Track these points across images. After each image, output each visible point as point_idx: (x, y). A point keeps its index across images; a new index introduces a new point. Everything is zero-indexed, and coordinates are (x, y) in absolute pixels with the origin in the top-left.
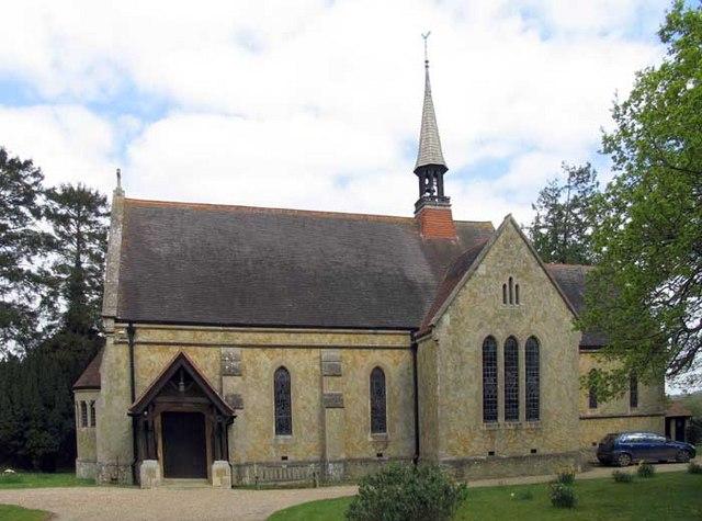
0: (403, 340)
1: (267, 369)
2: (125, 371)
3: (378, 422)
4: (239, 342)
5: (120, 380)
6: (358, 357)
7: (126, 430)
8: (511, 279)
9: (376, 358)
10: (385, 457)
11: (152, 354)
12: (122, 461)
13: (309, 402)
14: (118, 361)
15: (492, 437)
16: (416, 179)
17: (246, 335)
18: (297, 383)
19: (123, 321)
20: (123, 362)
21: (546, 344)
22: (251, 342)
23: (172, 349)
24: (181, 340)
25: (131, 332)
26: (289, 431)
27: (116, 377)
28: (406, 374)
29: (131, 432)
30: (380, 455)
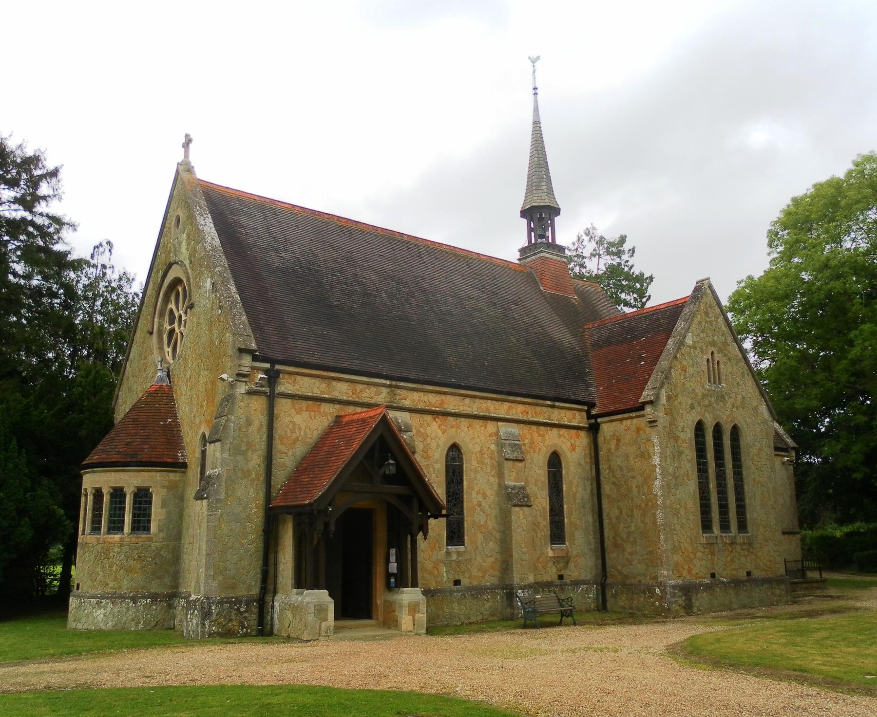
0: (578, 418)
1: (438, 446)
2: (259, 439)
3: (557, 534)
4: (407, 403)
5: (250, 454)
6: (535, 435)
7: (252, 537)
8: (712, 353)
9: (554, 439)
10: (567, 580)
11: (298, 413)
12: (242, 592)
13: (484, 495)
14: (249, 423)
15: (713, 554)
16: (524, 221)
17: (416, 396)
18: (470, 466)
19: (264, 360)
20: (256, 424)
21: (747, 437)
22: (420, 406)
23: (326, 407)
24: (336, 395)
25: (273, 377)
26: (461, 542)
27: (244, 448)
28: (583, 463)
29: (260, 544)
30: (561, 577)
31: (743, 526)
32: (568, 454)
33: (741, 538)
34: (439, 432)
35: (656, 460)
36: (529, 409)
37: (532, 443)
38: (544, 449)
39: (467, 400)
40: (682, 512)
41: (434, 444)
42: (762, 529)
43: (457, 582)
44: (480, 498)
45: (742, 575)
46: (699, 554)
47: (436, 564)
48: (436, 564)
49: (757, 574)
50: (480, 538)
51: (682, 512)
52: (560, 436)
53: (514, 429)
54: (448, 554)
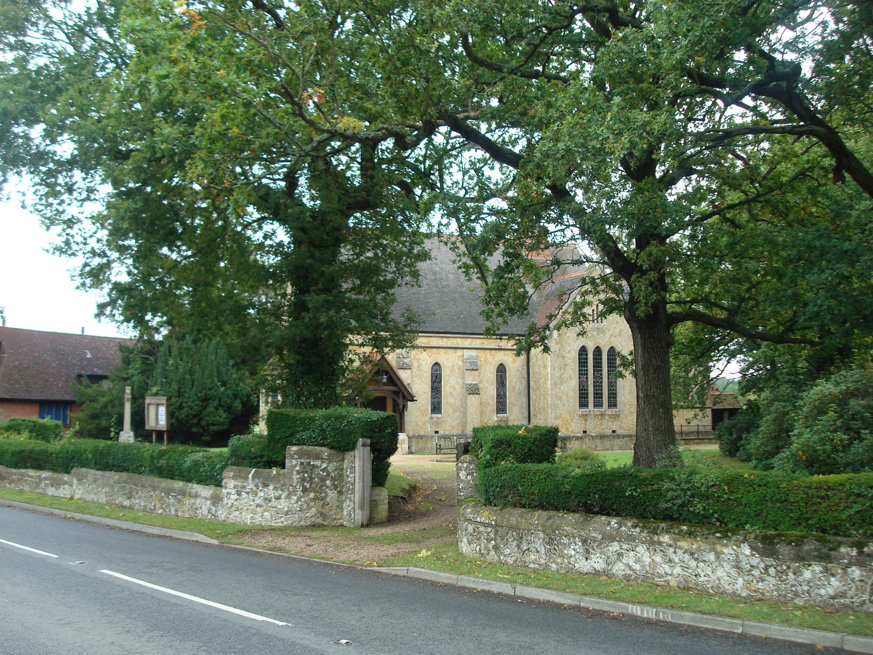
13: (454, 388)
15: (586, 420)
31: (613, 404)
32: (511, 365)
33: (610, 411)
34: (427, 357)
35: (549, 370)
36: (484, 341)
37: (486, 360)
38: (494, 363)
39: (445, 339)
40: (565, 397)
41: (424, 363)
42: (628, 407)
43: (437, 432)
44: (451, 390)
45: (609, 432)
46: (575, 420)
47: (424, 423)
48: (424, 423)
49: (619, 432)
50: (451, 410)
51: (565, 397)
52: (505, 355)
53: (473, 353)
54: (431, 418)
